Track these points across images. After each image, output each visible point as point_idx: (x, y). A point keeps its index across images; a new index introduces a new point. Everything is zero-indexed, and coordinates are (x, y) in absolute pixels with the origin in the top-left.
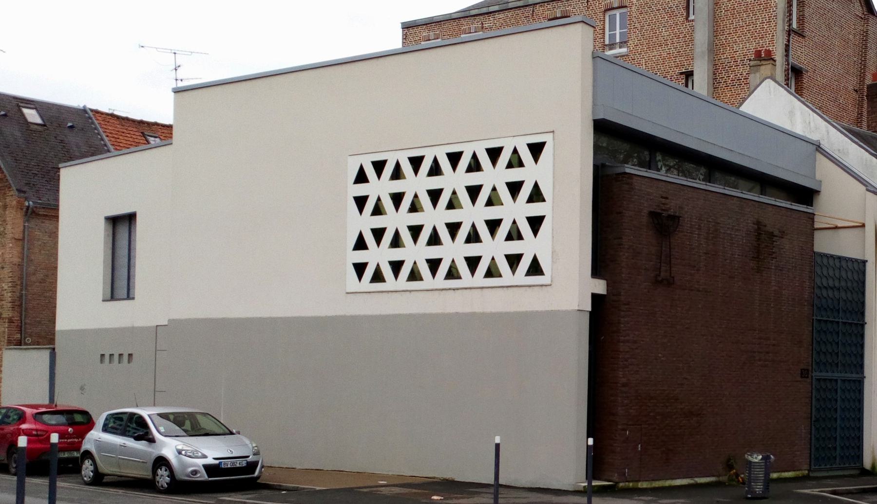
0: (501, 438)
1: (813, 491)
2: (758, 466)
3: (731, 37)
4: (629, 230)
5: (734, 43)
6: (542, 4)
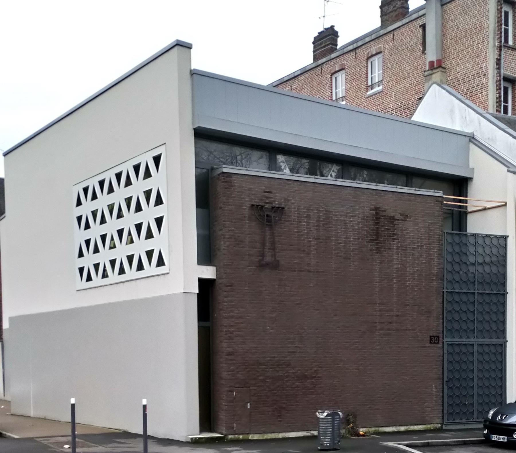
0: (147, 400)
1: (399, 444)
2: (326, 421)
3: (455, 61)
4: (229, 222)
5: (457, 65)
6: (327, 62)
